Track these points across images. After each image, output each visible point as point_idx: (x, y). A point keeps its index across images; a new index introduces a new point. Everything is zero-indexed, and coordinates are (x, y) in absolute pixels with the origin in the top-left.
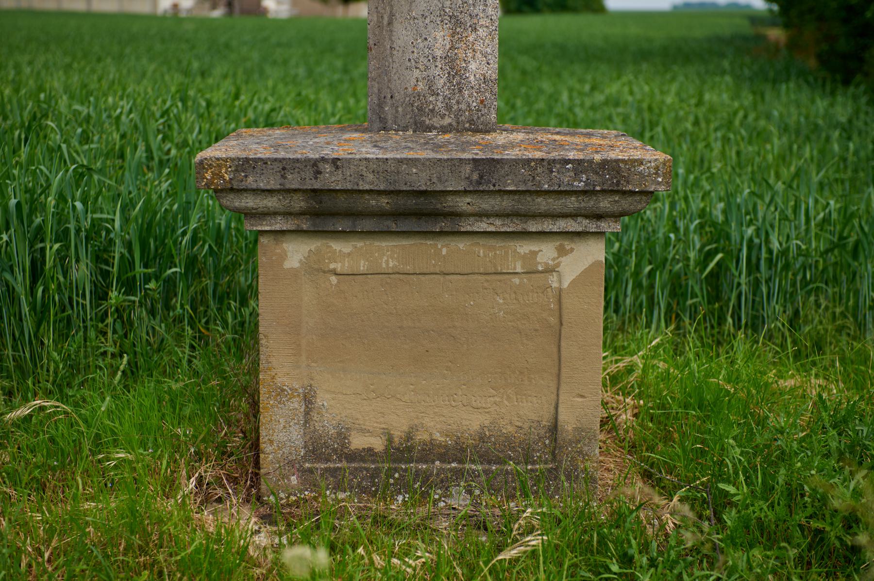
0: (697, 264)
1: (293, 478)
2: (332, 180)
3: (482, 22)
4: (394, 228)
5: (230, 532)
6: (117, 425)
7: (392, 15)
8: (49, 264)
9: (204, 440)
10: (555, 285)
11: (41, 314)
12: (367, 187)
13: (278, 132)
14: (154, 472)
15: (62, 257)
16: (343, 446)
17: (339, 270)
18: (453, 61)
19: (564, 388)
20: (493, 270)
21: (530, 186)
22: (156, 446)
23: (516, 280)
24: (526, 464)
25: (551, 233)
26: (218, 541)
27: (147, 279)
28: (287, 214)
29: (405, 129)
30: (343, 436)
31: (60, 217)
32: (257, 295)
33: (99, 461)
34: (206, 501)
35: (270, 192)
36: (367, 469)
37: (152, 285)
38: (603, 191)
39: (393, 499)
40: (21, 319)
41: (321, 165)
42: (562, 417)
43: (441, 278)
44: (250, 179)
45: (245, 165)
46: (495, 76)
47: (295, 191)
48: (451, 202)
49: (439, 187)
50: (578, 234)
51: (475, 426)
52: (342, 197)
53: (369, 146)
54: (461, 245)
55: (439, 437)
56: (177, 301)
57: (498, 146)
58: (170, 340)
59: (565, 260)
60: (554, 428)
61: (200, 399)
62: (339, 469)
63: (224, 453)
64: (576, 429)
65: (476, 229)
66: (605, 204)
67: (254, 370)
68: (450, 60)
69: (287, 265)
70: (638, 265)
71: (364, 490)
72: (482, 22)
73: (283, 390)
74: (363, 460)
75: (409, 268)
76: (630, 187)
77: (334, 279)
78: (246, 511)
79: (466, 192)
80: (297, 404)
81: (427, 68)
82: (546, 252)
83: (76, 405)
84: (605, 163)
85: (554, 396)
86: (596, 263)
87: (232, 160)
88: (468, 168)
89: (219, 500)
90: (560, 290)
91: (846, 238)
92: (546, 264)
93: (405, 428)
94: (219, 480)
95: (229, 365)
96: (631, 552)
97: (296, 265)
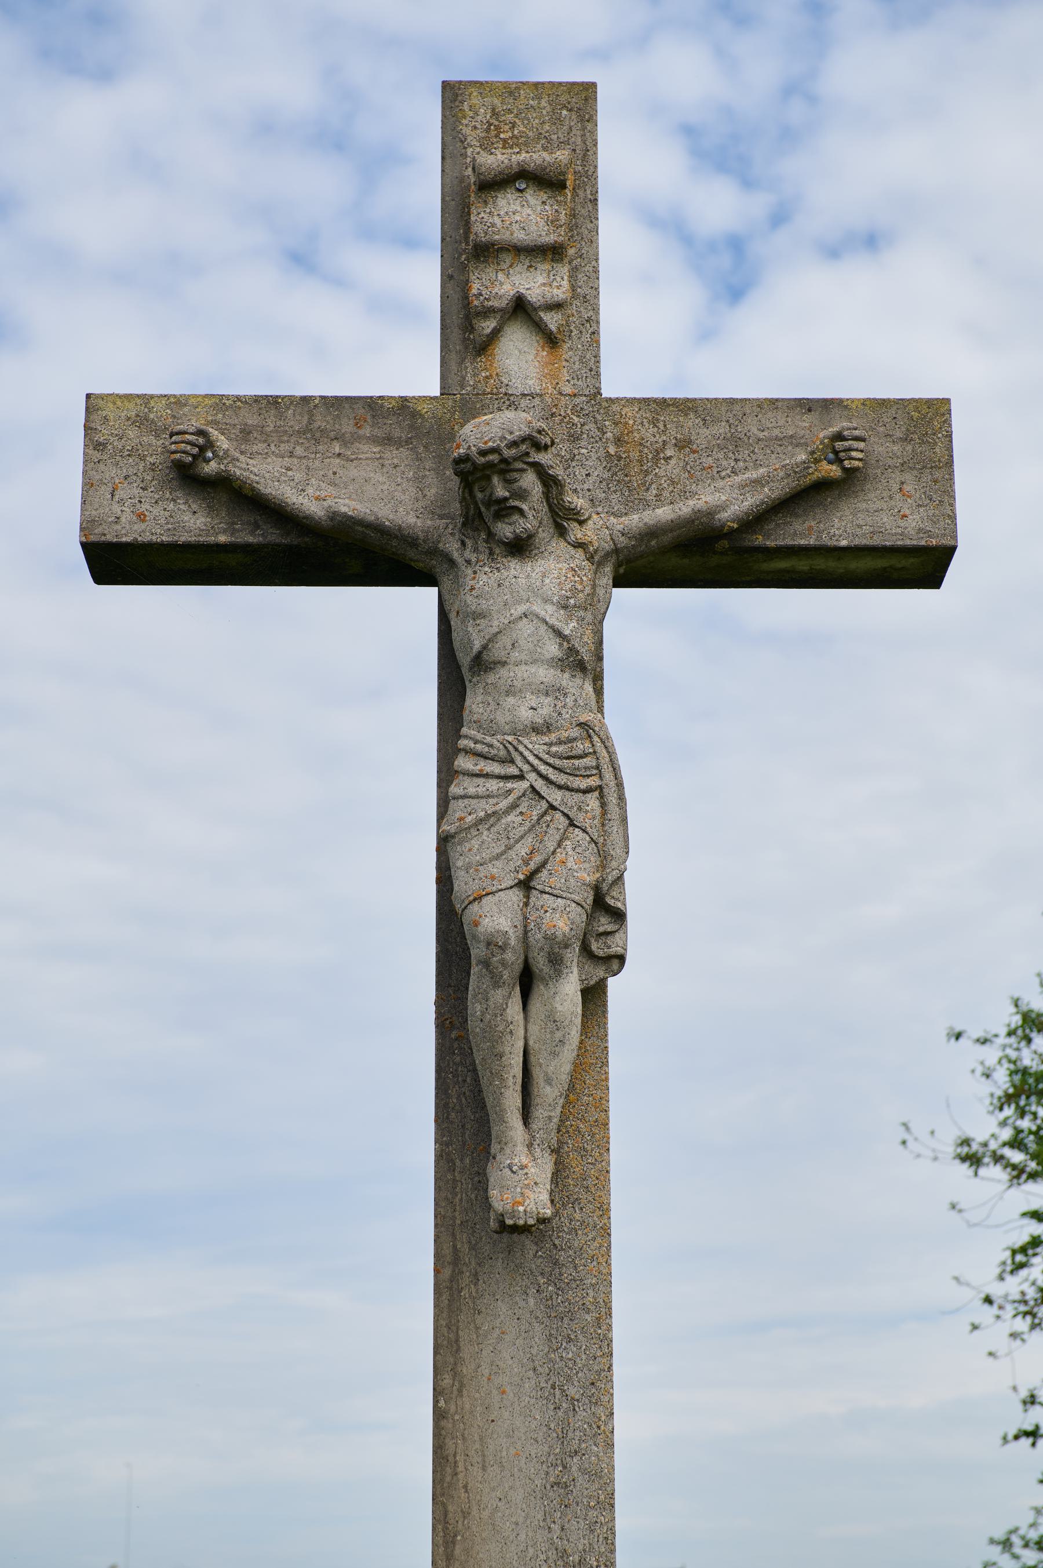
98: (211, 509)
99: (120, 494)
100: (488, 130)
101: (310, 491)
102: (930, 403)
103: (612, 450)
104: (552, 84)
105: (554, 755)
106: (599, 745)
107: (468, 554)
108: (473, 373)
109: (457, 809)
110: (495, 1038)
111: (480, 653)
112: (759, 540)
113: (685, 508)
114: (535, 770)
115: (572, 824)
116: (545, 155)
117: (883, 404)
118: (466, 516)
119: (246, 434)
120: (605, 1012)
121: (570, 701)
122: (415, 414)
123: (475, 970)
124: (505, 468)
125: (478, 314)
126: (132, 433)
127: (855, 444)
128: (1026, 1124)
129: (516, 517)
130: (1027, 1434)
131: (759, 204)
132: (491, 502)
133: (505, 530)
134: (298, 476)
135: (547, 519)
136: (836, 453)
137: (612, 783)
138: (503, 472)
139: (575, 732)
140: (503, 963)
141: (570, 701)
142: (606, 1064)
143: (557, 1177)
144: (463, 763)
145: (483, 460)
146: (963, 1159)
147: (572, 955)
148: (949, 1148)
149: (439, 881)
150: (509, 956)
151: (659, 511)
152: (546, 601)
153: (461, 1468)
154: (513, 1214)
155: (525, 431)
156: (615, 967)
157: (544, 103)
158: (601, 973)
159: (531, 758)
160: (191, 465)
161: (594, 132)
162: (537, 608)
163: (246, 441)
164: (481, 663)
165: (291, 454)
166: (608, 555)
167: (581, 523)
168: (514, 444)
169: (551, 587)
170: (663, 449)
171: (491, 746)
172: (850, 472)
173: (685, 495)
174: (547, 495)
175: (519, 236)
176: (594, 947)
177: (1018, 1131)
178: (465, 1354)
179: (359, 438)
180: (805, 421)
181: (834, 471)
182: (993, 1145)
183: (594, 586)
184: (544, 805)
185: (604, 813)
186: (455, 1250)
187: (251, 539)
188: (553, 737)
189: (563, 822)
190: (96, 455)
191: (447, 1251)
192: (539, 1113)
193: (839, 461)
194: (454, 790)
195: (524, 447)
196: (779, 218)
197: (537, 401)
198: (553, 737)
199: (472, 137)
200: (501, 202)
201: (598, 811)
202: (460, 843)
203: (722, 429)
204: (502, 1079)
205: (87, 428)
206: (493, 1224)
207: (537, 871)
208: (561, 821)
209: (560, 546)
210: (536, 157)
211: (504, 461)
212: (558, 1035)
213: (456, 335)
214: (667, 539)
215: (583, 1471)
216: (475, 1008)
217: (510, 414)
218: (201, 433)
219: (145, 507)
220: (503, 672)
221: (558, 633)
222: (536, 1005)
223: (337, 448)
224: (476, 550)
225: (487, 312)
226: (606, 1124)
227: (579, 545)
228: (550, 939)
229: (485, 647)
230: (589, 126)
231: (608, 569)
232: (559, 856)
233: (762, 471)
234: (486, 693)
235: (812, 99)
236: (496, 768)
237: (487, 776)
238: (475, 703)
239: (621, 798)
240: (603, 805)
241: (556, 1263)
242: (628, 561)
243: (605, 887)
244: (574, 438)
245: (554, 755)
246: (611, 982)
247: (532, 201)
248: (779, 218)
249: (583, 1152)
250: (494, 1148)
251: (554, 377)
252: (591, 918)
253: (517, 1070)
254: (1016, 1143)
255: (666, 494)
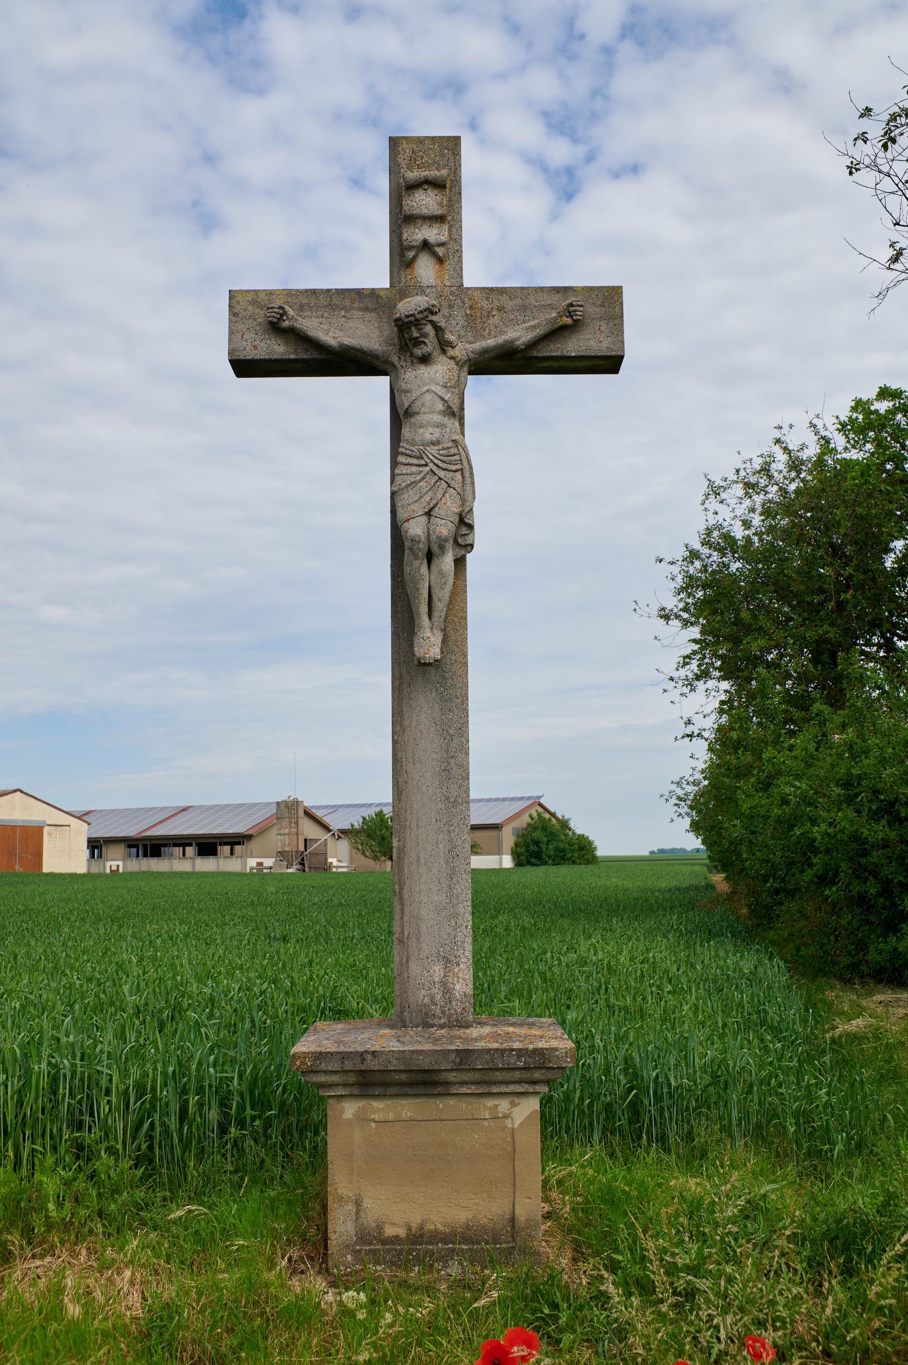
0: (621, 1098)
1: (349, 1256)
2: (372, 1064)
3: (462, 960)
4: (410, 1092)
5: (309, 1292)
6: (238, 1222)
7: (408, 957)
8: (191, 1111)
9: (292, 1232)
10: (510, 1126)
11: (186, 1147)
12: (393, 1068)
13: (339, 1026)
14: (261, 1254)
15: (201, 1105)
16: (380, 1234)
17: (376, 1119)
18: (445, 984)
19: (518, 1193)
20: (471, 1117)
21: (491, 1066)
22: (262, 1236)
23: (486, 1123)
24: (496, 1244)
25: (506, 1093)
26: (303, 1299)
27: (253, 1119)
28: (345, 1085)
29: (417, 1026)
30: (380, 1228)
31: (200, 1080)
32: (325, 1129)
33: (227, 1247)
34: (294, 1272)
35: (335, 1072)
36: (395, 1250)
37: (257, 1123)
38: (535, 1068)
39: (411, 1270)
40: (172, 1148)
41: (365, 1055)
42: (517, 1212)
43: (440, 1123)
44: (323, 1065)
45: (320, 1056)
46: (471, 993)
47: (350, 1071)
48: (443, 1076)
49: (436, 1068)
50: (523, 1094)
51: (463, 1220)
52: (378, 1074)
53: (395, 1040)
54: (452, 1101)
55: (440, 1227)
56: (272, 1131)
57: (472, 1039)
58: (268, 1160)
59: (515, 1110)
60: (513, 1220)
61: (289, 1203)
62: (375, 1250)
63: (304, 1240)
64: (526, 1220)
65: (459, 1092)
66: (537, 1075)
67: (324, 1182)
68: (444, 984)
69: (345, 1116)
70: (582, 1099)
71: (393, 1264)
72: (462, 960)
73: (342, 1198)
74: (393, 1243)
75: (419, 1117)
76: (551, 1065)
77: (373, 1125)
78: (319, 1279)
79: (452, 1070)
80: (351, 1207)
81: (430, 989)
82: (504, 1105)
83: (209, 1208)
84: (535, 1050)
85: (512, 1198)
86: (534, 1112)
87: (312, 1053)
88: (453, 1056)
89: (302, 1272)
90: (513, 1129)
91: (719, 1077)
92: (504, 1112)
93: (419, 1221)
94: (302, 1258)
95: (308, 1179)
96: (557, 1301)
97: (350, 1116)
98: (286, 343)
99: (245, 337)
100: (410, 160)
101: (331, 334)
102: (613, 288)
103: (468, 312)
104: (440, 137)
105: (441, 455)
106: (461, 450)
107: (401, 363)
108: (405, 277)
109: (398, 479)
110: (416, 582)
111: (407, 409)
112: (535, 353)
113: (501, 340)
114: (432, 462)
115: (449, 486)
116: (436, 172)
117: (591, 289)
118: (401, 346)
119: (302, 307)
120: (465, 569)
121: (448, 430)
122: (378, 297)
123: (407, 552)
124: (417, 323)
125: (406, 249)
126: (250, 308)
127: (578, 308)
128: (690, 601)
129: (423, 346)
130: (688, 736)
131: (580, 151)
132: (412, 339)
133: (418, 352)
134: (325, 327)
135: (437, 347)
136: (570, 312)
137: (467, 467)
138: (416, 325)
139: (450, 444)
140: (419, 549)
141: (448, 430)
142: (466, 592)
143: (444, 641)
144: (401, 459)
145: (407, 320)
146: (661, 617)
147: (449, 545)
148: (654, 610)
149: (391, 512)
150: (421, 546)
151: (489, 341)
152: (437, 384)
153: (404, 763)
154: (424, 658)
155: (426, 306)
156: (469, 549)
157: (436, 147)
158: (463, 552)
159: (431, 457)
160: (277, 323)
161: (460, 160)
162: (433, 388)
163: (302, 311)
164: (409, 413)
165: (322, 317)
166: (465, 362)
167: (453, 347)
168: (421, 312)
169: (439, 378)
170: (491, 311)
171: (413, 451)
172: (576, 321)
173: (502, 333)
174: (437, 335)
175: (425, 211)
176: (460, 540)
177: (687, 604)
178: (406, 716)
179: (353, 308)
180: (557, 297)
181: (569, 321)
182: (675, 610)
183: (459, 377)
184: (437, 478)
185: (463, 481)
186: (401, 673)
187: (305, 357)
188: (441, 447)
189: (445, 485)
190: (234, 319)
191: (397, 673)
192: (436, 614)
193: (571, 316)
194: (397, 471)
195: (425, 313)
196: (590, 158)
197: (434, 289)
198: (441, 447)
199: (403, 164)
200: (417, 195)
201: (461, 480)
202: (400, 495)
203: (518, 302)
204: (419, 600)
205: (230, 306)
206: (416, 663)
207: (434, 507)
208: (444, 485)
209: (443, 359)
210: (433, 173)
211: (416, 320)
212: (443, 580)
213: (397, 258)
214: (492, 354)
215: (456, 764)
216: (407, 569)
217: (419, 298)
218: (281, 308)
219: (257, 342)
220: (418, 417)
221: (443, 399)
222: (434, 567)
223: (343, 313)
224: (405, 361)
225: (410, 248)
226: (466, 618)
227: (452, 358)
228: (439, 538)
229: (410, 406)
230: (457, 157)
231: (466, 369)
232: (443, 501)
233: (536, 321)
234: (411, 427)
235: (606, 98)
236: (415, 461)
237: (411, 465)
238: (406, 432)
239: (472, 474)
240: (463, 477)
241: (444, 678)
242: (475, 364)
243: (464, 514)
244: (451, 307)
245: (441, 455)
246: (468, 555)
247: (431, 194)
248: (590, 158)
249: (456, 631)
250: (416, 630)
251: (441, 278)
252: (458, 528)
253: (426, 596)
254: (685, 609)
255: (493, 332)
